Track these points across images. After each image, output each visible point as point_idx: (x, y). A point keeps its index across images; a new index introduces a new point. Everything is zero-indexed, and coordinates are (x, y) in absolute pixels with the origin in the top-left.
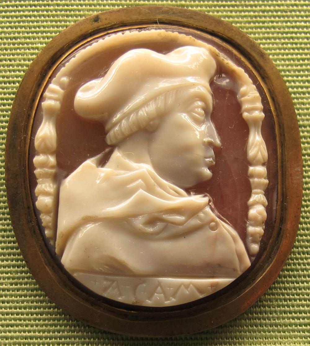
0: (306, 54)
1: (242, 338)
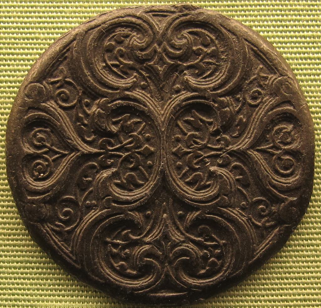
0: (317, 294)
1: (255, 280)
